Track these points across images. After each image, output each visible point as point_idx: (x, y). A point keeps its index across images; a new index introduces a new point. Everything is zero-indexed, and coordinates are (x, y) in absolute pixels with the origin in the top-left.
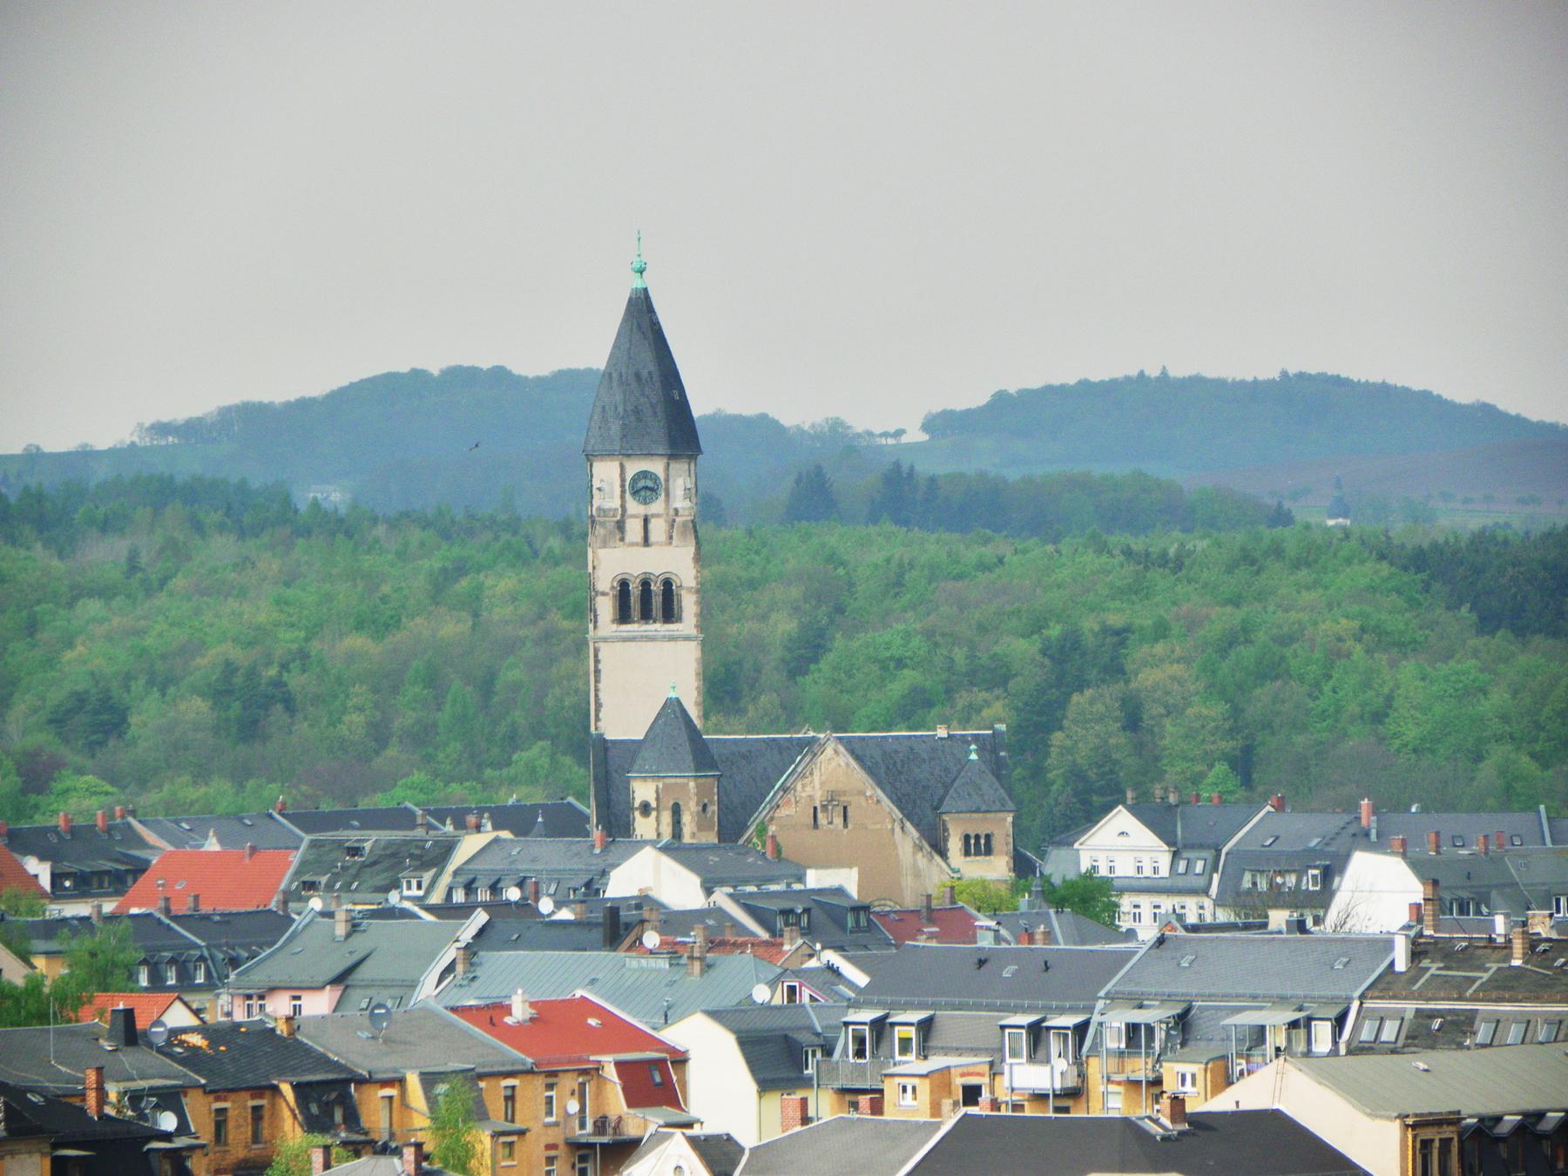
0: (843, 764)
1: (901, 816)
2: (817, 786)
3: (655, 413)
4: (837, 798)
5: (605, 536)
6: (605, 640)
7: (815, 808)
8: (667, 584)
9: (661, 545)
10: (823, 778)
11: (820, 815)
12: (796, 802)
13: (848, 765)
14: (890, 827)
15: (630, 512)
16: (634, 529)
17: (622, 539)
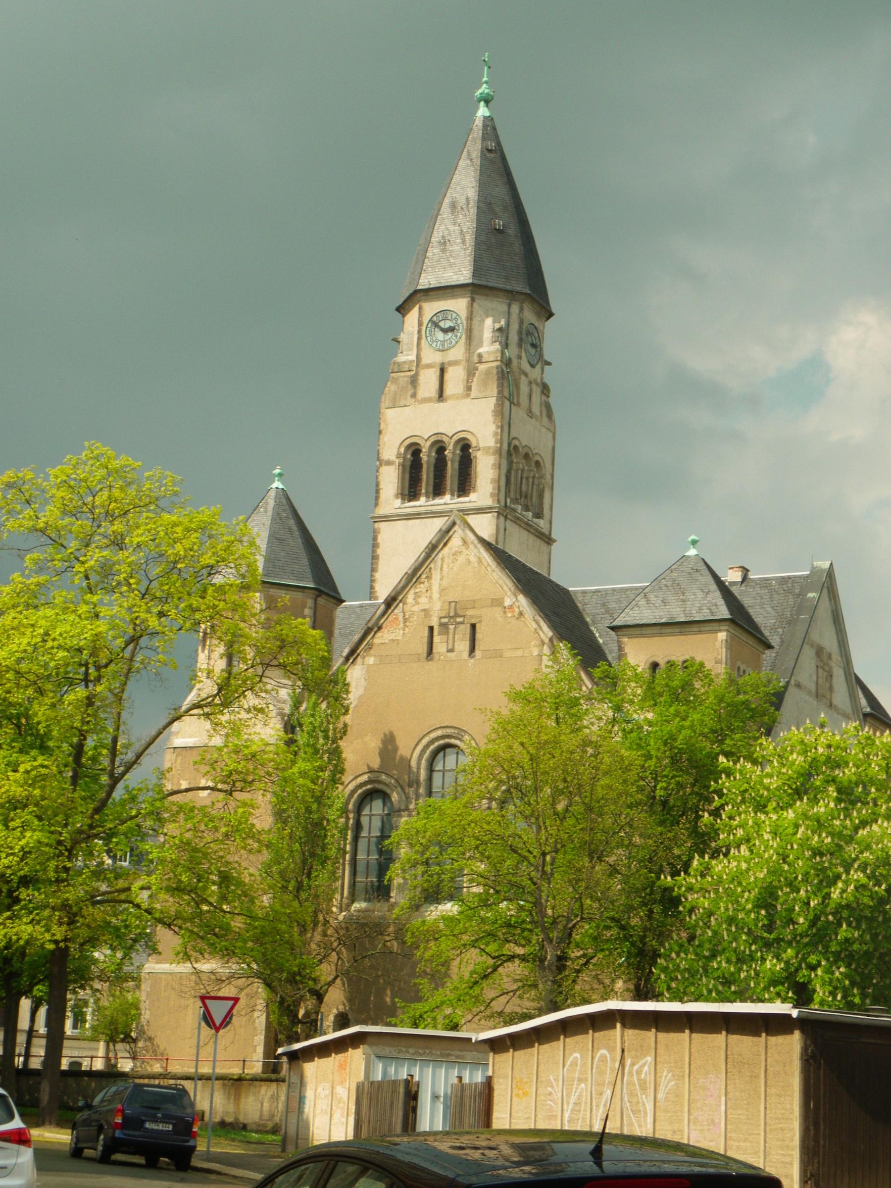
0: (473, 559)
1: (550, 634)
2: (436, 595)
3: (464, 242)
4: (460, 612)
5: (395, 394)
6: (386, 518)
7: (431, 629)
8: (465, 447)
9: (458, 398)
10: (444, 583)
11: (437, 639)
12: (405, 620)
13: (480, 561)
14: (536, 653)
15: (425, 360)
16: (428, 381)
17: (414, 395)
